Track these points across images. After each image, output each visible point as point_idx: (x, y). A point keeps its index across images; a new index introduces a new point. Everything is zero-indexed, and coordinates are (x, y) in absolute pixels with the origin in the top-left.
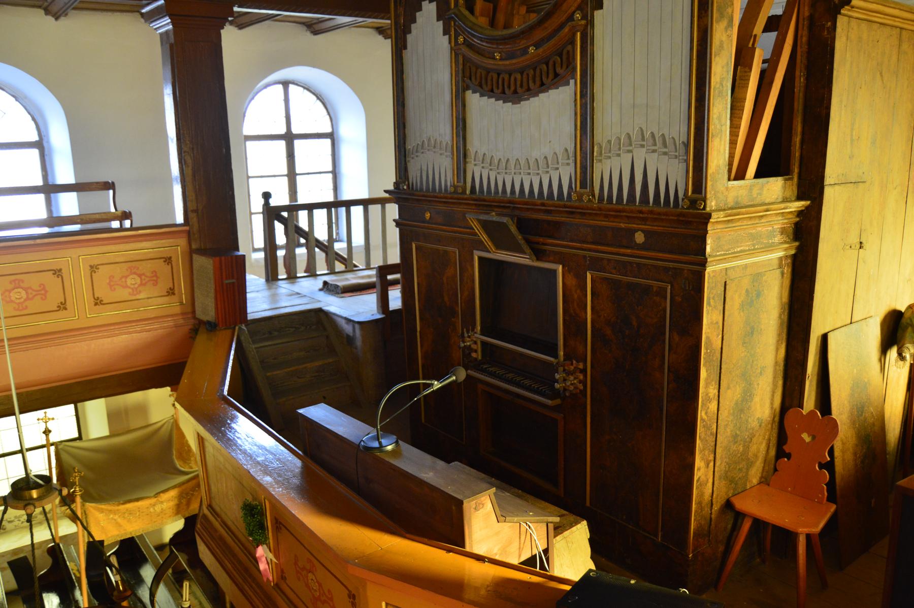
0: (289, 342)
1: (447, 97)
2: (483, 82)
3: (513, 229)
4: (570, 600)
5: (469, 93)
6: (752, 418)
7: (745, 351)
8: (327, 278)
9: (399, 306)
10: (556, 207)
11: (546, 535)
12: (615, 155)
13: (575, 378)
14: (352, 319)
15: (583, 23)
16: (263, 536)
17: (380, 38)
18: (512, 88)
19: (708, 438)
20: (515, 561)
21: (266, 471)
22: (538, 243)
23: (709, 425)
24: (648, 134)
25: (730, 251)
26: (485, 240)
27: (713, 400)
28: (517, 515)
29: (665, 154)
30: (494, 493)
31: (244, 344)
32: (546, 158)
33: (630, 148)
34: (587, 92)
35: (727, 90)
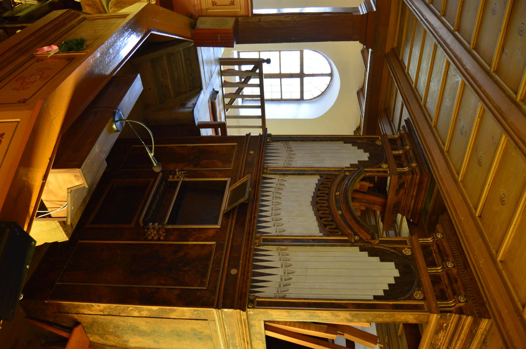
0: (183, 69)
1: (317, 165)
2: (324, 185)
3: (241, 200)
4: (17, 230)
5: (318, 177)
6: (129, 337)
7: (168, 332)
8: (220, 93)
9: (202, 134)
10: (253, 225)
11: (60, 216)
12: (280, 258)
13: (155, 234)
14: (196, 107)
15: (352, 241)
16: (64, 50)
17: (354, 129)
18: (320, 202)
19: (117, 311)
20: (43, 197)
21: (104, 54)
22: (233, 214)
23: (125, 311)
24: (291, 276)
25: (225, 322)
26: (236, 185)
27: (139, 313)
28: (72, 200)
29: (280, 286)
30: (85, 186)
31: (182, 44)
32: (281, 219)
33: (284, 266)
34: (316, 242)
35: (313, 320)
